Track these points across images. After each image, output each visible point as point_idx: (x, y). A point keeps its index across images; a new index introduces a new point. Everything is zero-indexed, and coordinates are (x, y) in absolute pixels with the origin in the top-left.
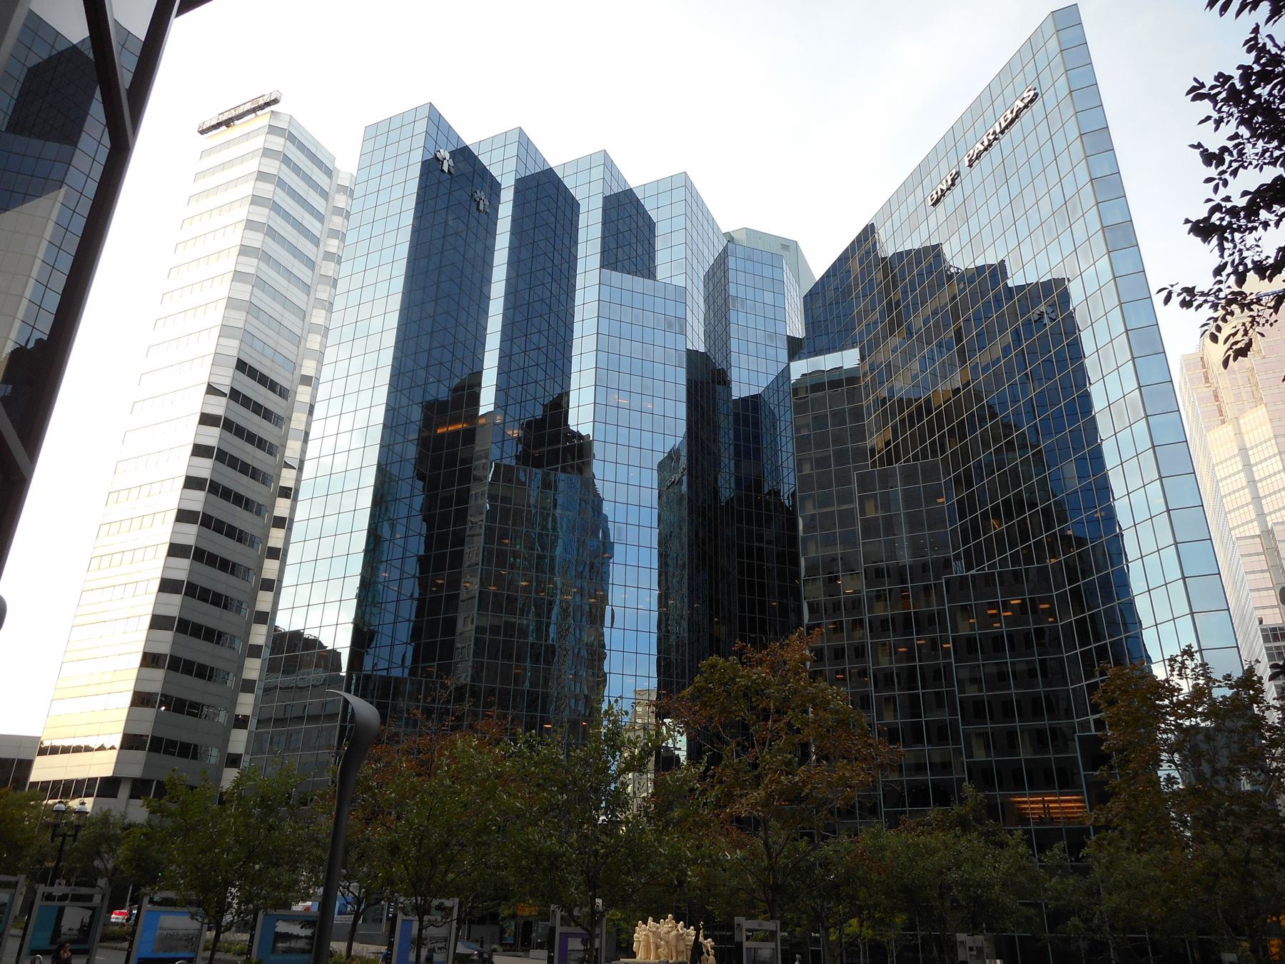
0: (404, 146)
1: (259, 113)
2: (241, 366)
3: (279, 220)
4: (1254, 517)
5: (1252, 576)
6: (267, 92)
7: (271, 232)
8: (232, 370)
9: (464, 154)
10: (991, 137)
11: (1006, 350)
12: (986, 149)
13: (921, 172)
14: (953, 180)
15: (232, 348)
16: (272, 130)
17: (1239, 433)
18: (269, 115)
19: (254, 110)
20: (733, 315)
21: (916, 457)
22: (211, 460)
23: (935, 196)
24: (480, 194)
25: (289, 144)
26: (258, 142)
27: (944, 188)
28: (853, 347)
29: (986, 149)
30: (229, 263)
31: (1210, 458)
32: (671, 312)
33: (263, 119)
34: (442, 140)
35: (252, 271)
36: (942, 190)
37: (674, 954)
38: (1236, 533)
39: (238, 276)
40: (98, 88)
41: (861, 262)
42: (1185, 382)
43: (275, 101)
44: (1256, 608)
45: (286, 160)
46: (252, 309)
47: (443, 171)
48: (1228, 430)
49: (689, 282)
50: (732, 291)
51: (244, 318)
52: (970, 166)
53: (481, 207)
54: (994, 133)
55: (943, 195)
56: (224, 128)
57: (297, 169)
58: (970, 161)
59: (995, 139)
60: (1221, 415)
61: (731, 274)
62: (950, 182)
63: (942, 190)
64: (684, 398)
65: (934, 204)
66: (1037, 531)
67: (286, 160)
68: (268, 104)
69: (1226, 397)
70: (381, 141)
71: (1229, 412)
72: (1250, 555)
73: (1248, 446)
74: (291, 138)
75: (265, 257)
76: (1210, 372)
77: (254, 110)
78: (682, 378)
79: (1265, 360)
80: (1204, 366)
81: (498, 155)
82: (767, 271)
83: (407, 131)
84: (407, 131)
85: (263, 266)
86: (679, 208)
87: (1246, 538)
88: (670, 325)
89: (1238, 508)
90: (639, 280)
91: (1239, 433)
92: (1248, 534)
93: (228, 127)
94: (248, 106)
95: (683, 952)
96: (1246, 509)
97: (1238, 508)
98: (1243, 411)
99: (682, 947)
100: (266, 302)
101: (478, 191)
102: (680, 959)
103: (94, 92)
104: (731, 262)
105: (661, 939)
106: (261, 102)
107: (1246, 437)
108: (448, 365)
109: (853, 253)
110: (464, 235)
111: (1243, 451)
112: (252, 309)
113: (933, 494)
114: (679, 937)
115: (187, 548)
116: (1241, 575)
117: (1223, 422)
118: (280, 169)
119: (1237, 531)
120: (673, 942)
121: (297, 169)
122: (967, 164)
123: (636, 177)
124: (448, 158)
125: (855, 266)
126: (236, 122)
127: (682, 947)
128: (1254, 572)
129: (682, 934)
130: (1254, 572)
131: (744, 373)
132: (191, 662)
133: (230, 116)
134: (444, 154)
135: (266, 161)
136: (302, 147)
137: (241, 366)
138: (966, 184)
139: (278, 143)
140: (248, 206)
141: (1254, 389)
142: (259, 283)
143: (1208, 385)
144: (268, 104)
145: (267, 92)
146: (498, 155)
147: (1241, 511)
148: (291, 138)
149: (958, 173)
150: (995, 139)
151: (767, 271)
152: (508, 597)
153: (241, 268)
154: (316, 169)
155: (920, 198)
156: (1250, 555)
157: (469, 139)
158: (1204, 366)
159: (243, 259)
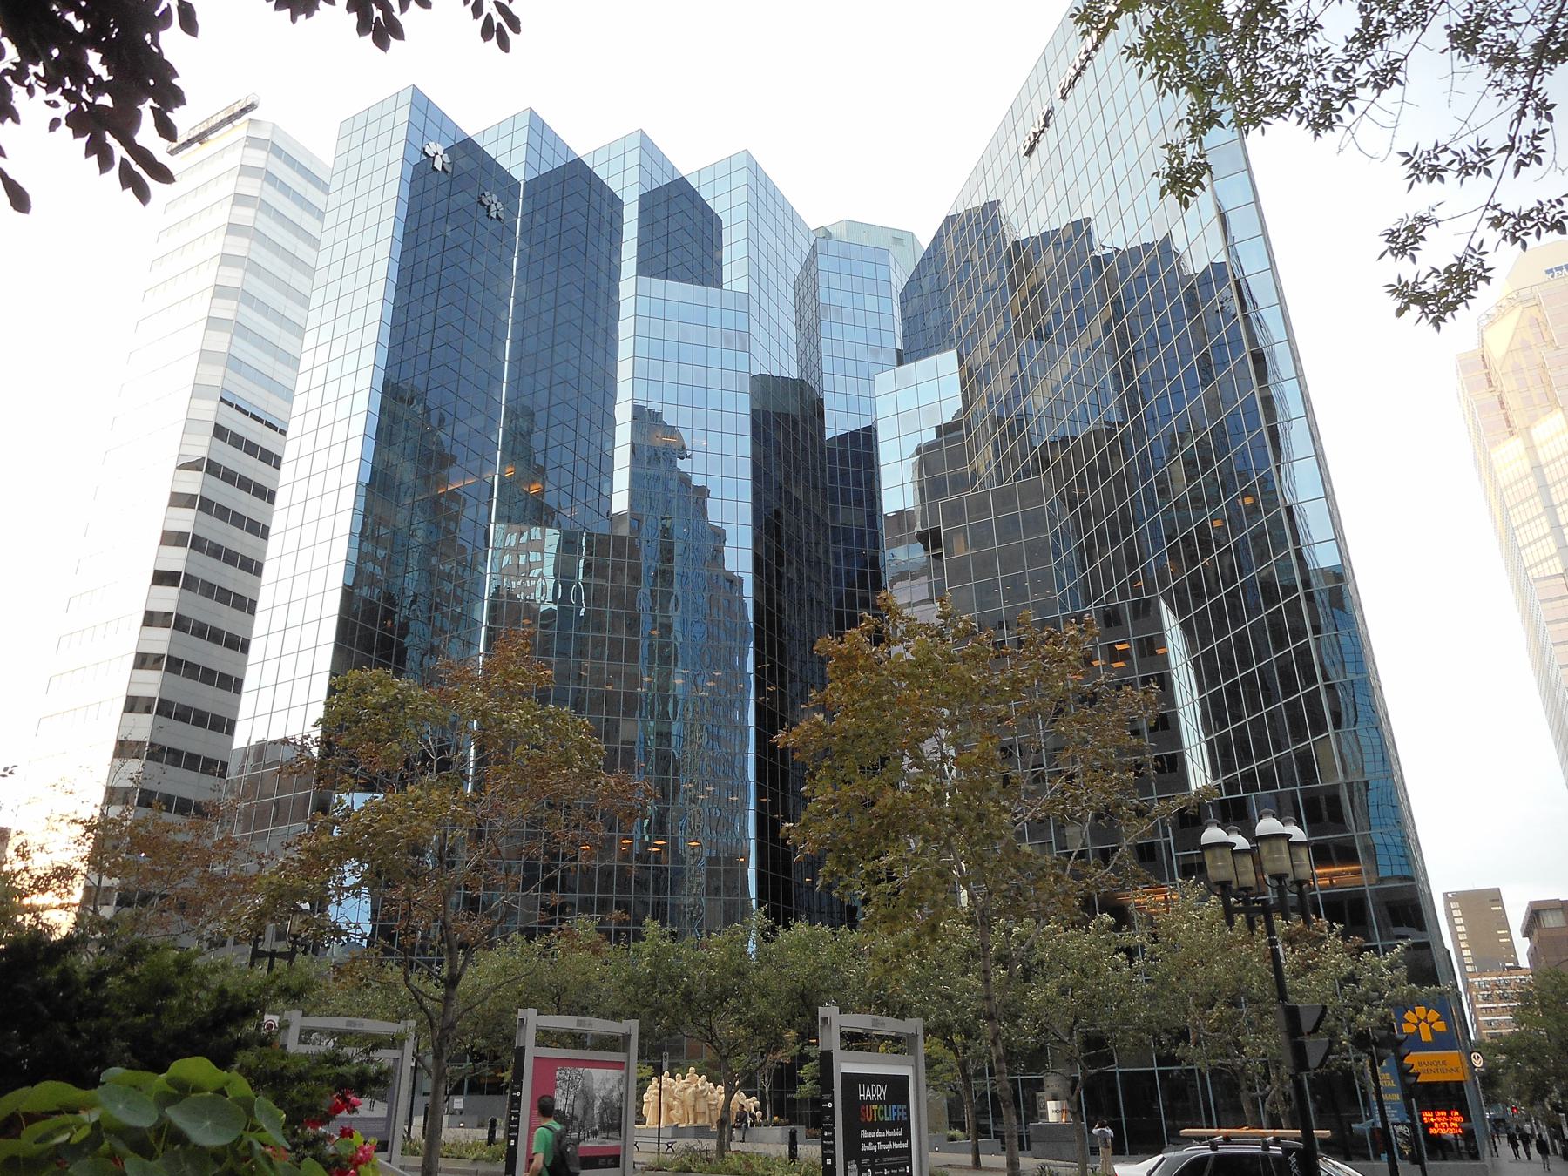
0: (384, 141)
1: (236, 122)
2: (220, 432)
3: (264, 252)
4: (1554, 551)
5: (1556, 627)
6: (239, 97)
7: (252, 267)
8: (207, 439)
9: (466, 148)
10: (1083, 57)
11: (1107, 328)
12: (1078, 74)
13: (1013, 115)
14: (1046, 119)
15: (209, 411)
16: (252, 142)
17: (1531, 448)
18: (246, 125)
19: (230, 119)
20: (824, 325)
21: (1017, 477)
22: (185, 549)
23: (1028, 143)
24: (491, 198)
25: (273, 158)
26: (234, 158)
27: (1037, 131)
28: (950, 349)
29: (1078, 74)
30: (202, 307)
31: (1496, 482)
32: (729, 325)
33: (240, 128)
34: (432, 130)
35: (230, 315)
36: (1035, 134)
37: (691, 1116)
38: (1533, 573)
39: (213, 323)
40: (107, 133)
41: (956, 239)
42: (1463, 388)
43: (252, 106)
44: (1561, 667)
45: (270, 178)
46: (233, 363)
47: (434, 169)
48: (1516, 445)
49: (753, 284)
50: (823, 296)
51: (221, 374)
52: (1064, 98)
53: (493, 215)
54: (1086, 52)
55: (1037, 141)
56: (196, 145)
57: (285, 189)
58: (1062, 92)
59: (1088, 58)
60: (1509, 426)
61: (822, 277)
62: (1042, 123)
63: (1035, 134)
64: (748, 430)
65: (1028, 153)
66: (1145, 556)
67: (270, 178)
68: (244, 111)
69: (1512, 402)
70: (357, 139)
71: (1517, 421)
72: (1551, 600)
73: (1543, 462)
74: (276, 150)
75: (246, 298)
76: (1492, 372)
77: (230, 119)
78: (745, 407)
79: (1559, 352)
80: (1485, 366)
81: (505, 144)
82: (869, 271)
83: (387, 123)
84: (387, 123)
85: (244, 309)
86: (740, 195)
87: (1546, 578)
88: (728, 342)
89: (1535, 542)
90: (701, 289)
91: (1531, 448)
92: (1548, 574)
93: (201, 143)
94: (222, 116)
95: (704, 1113)
96: (1544, 541)
97: (1535, 542)
98: (1534, 418)
99: (702, 1106)
100: (249, 353)
101: (487, 193)
102: (700, 1123)
103: (105, 139)
104: (822, 263)
105: (675, 1099)
106: (237, 109)
107: (1540, 452)
108: (571, 446)
109: (948, 230)
110: (468, 247)
111: (1537, 468)
112: (233, 363)
113: (1034, 522)
114: (698, 1095)
115: (159, 658)
116: (1542, 626)
117: (1512, 434)
118: (262, 188)
119: (1534, 570)
120: (690, 1101)
121: (285, 189)
122: (1059, 95)
123: (688, 160)
124: (441, 153)
125: (949, 247)
126: (210, 137)
127: (702, 1106)
128: (1558, 621)
129: (703, 1091)
130: (1558, 621)
131: (841, 399)
132: (151, 792)
133: (202, 130)
134: (434, 148)
135: (245, 180)
136: (291, 162)
137: (220, 432)
138: (1058, 121)
139: (258, 158)
140: (222, 237)
141: (1548, 389)
142: (240, 329)
143: (1492, 389)
144: (244, 111)
145: (242, 97)
146: (505, 144)
147: (1539, 544)
148: (276, 150)
149: (1051, 111)
150: (1088, 58)
151: (869, 271)
152: (371, 653)
153: (216, 313)
154: (310, 187)
155: (1013, 150)
156: (1551, 600)
157: (471, 129)
158: (1485, 366)
159: (218, 302)
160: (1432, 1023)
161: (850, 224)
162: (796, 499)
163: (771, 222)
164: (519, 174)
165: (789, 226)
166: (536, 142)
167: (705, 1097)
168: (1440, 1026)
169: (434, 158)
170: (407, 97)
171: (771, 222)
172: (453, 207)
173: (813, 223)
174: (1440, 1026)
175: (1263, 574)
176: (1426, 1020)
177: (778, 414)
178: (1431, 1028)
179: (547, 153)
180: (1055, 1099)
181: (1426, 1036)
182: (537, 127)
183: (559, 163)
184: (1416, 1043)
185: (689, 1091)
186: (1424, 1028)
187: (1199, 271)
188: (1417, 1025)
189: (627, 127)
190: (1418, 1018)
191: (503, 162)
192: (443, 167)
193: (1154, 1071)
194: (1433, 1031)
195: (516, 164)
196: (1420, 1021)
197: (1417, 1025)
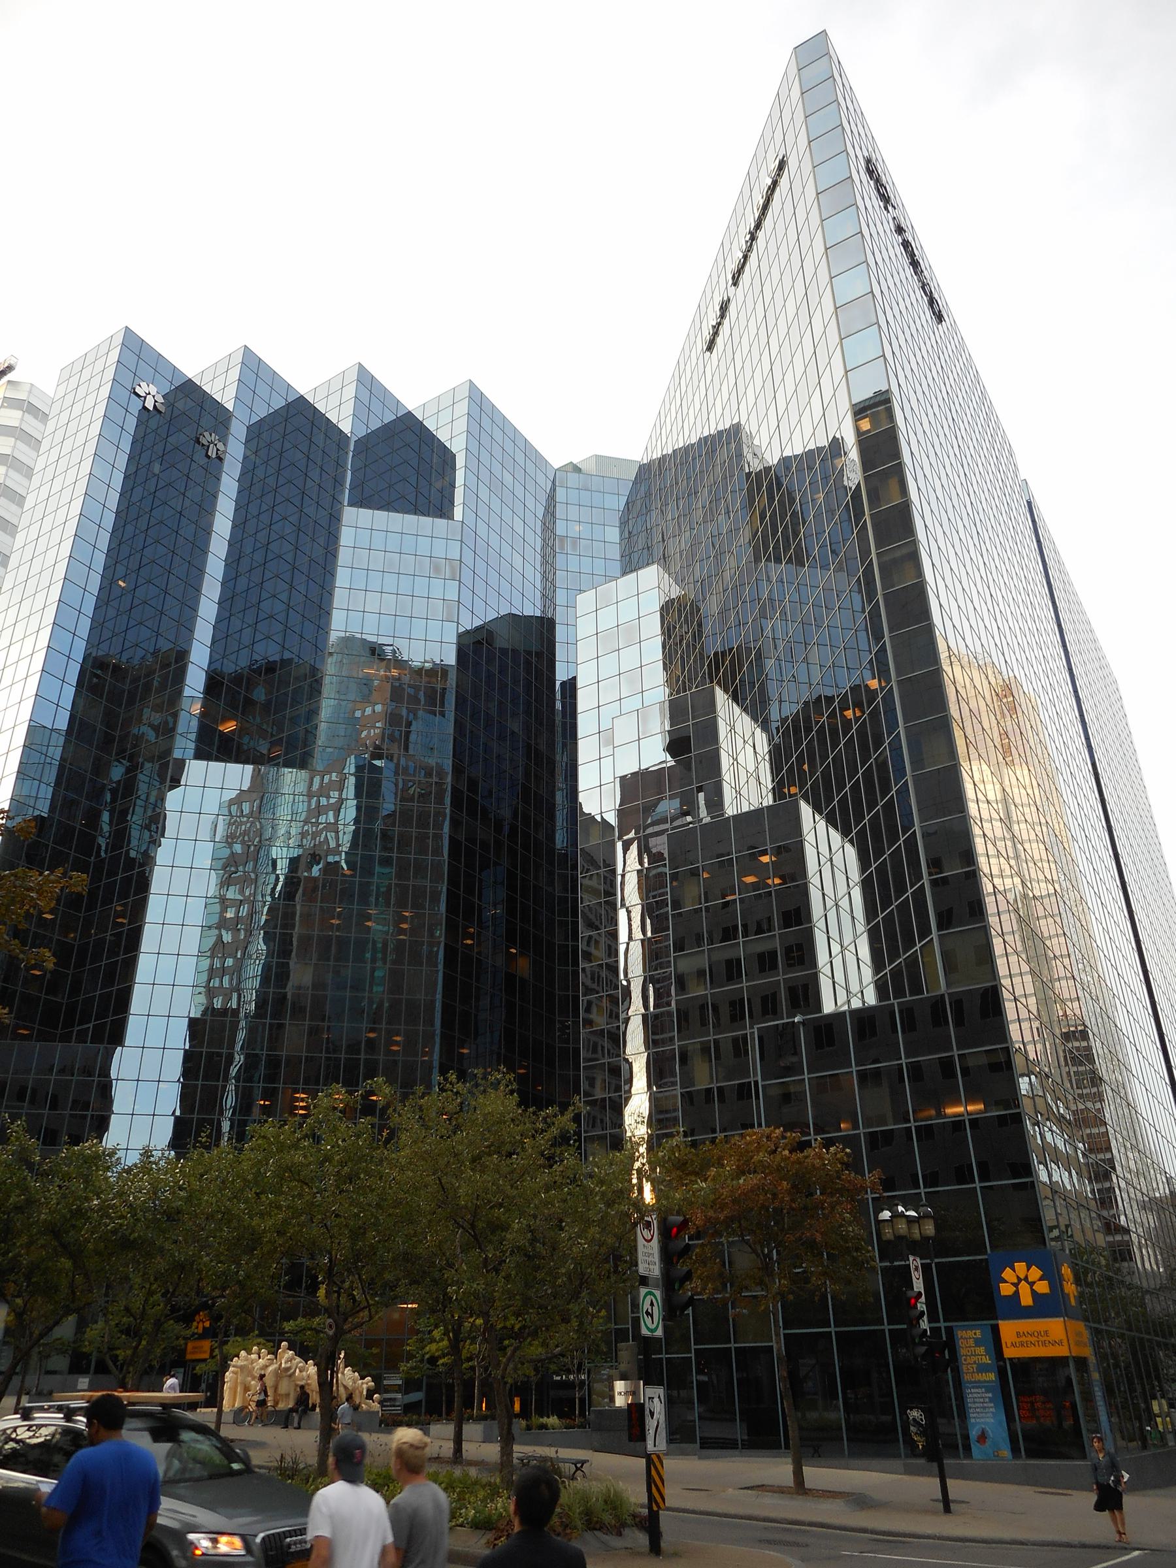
81: (334, 401)
83: (99, 365)
86: (462, 425)
88: (437, 569)
104: (560, 494)
146: (445, 417)
157: (191, 370)
160: (1034, 1283)
161: (599, 458)
162: (513, 733)
163: (497, 452)
164: (346, 427)
165: (520, 458)
166: (131, 360)
167: (290, 1376)
168: (1043, 1287)
169: (145, 398)
170: (119, 339)
171: (497, 452)
172: (169, 447)
173: (557, 460)
174: (1043, 1287)
175: (279, 748)
176: (1026, 1279)
177: (529, 653)
178: (1032, 1290)
179: (376, 407)
180: (623, 1377)
181: (1026, 1300)
182: (366, 380)
183: (389, 417)
184: (1014, 1309)
185: (271, 1369)
186: (1024, 1288)
187: (775, 462)
188: (1016, 1285)
189: (457, 379)
190: (1018, 1277)
191: (332, 417)
192: (155, 405)
193: (831, 1332)
194: (1033, 1292)
195: (224, 391)
196: (1020, 1280)
197: (1016, 1285)
